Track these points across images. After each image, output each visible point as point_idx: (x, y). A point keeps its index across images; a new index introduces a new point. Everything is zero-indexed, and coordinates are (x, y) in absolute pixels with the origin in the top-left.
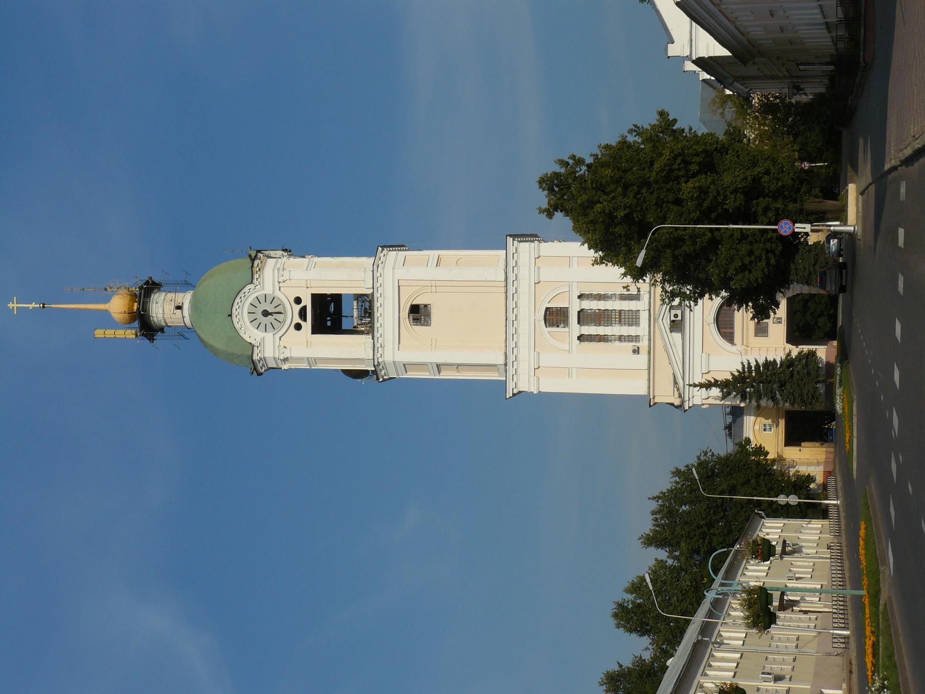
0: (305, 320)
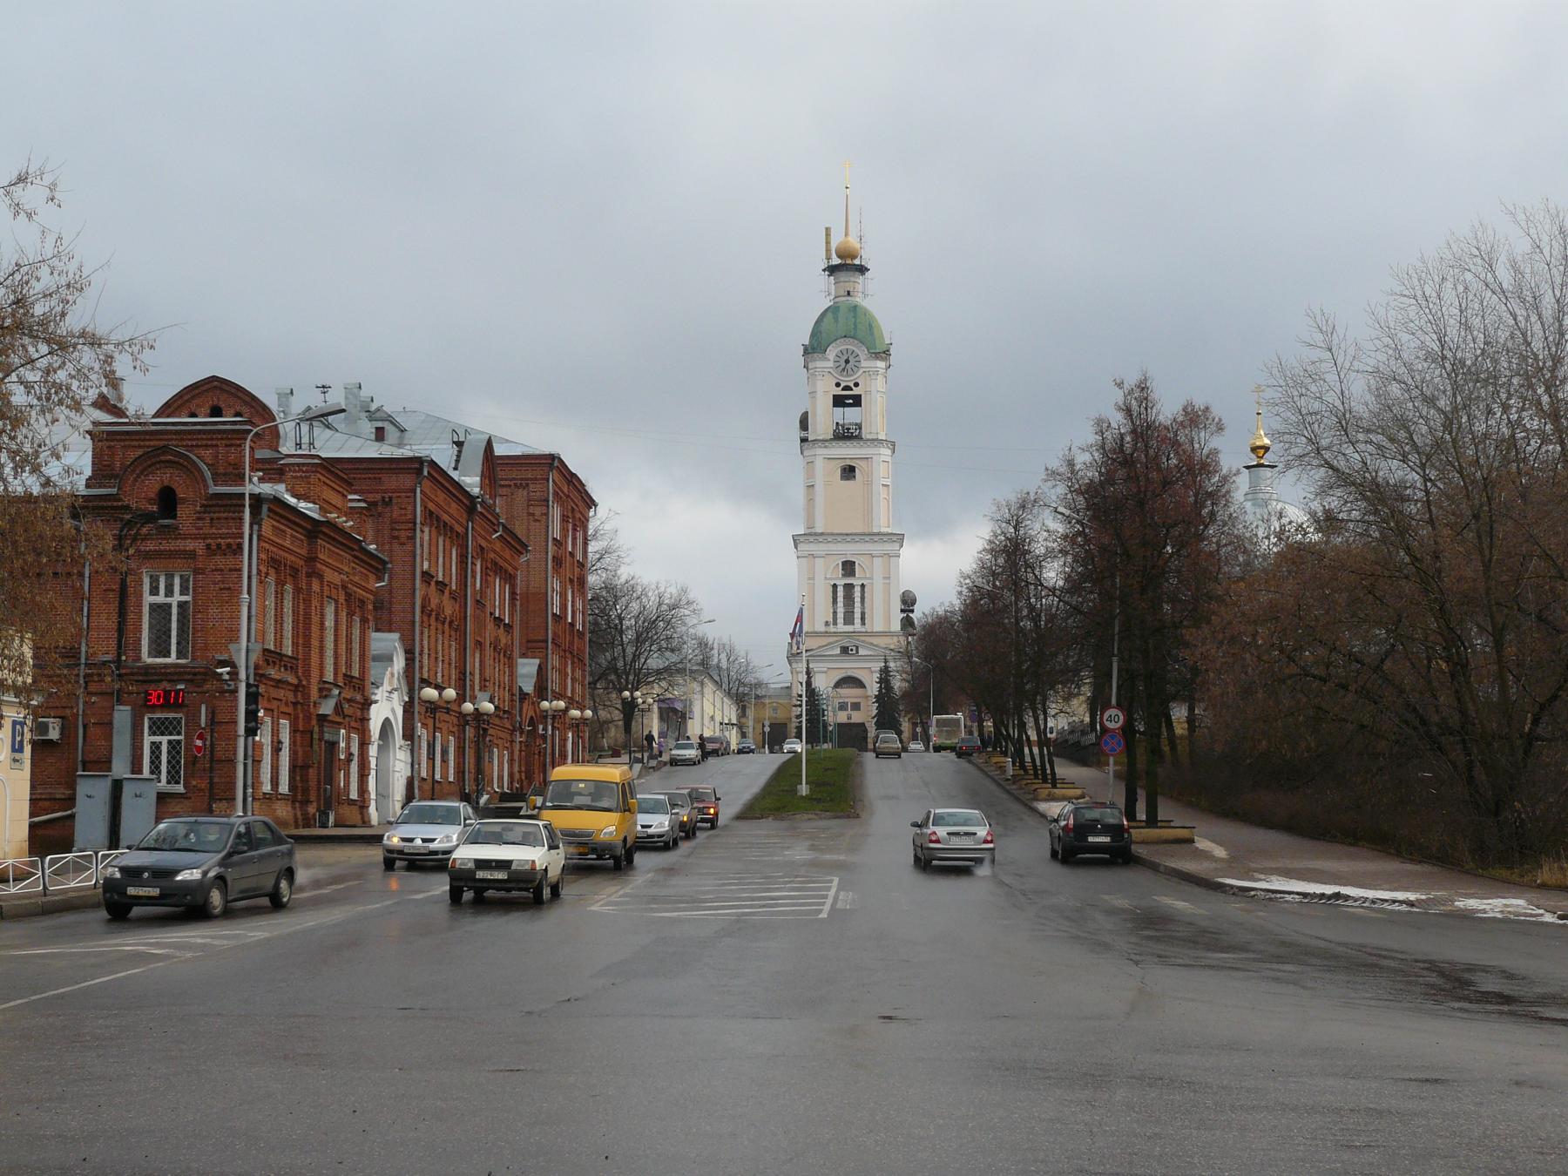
0: (843, 389)
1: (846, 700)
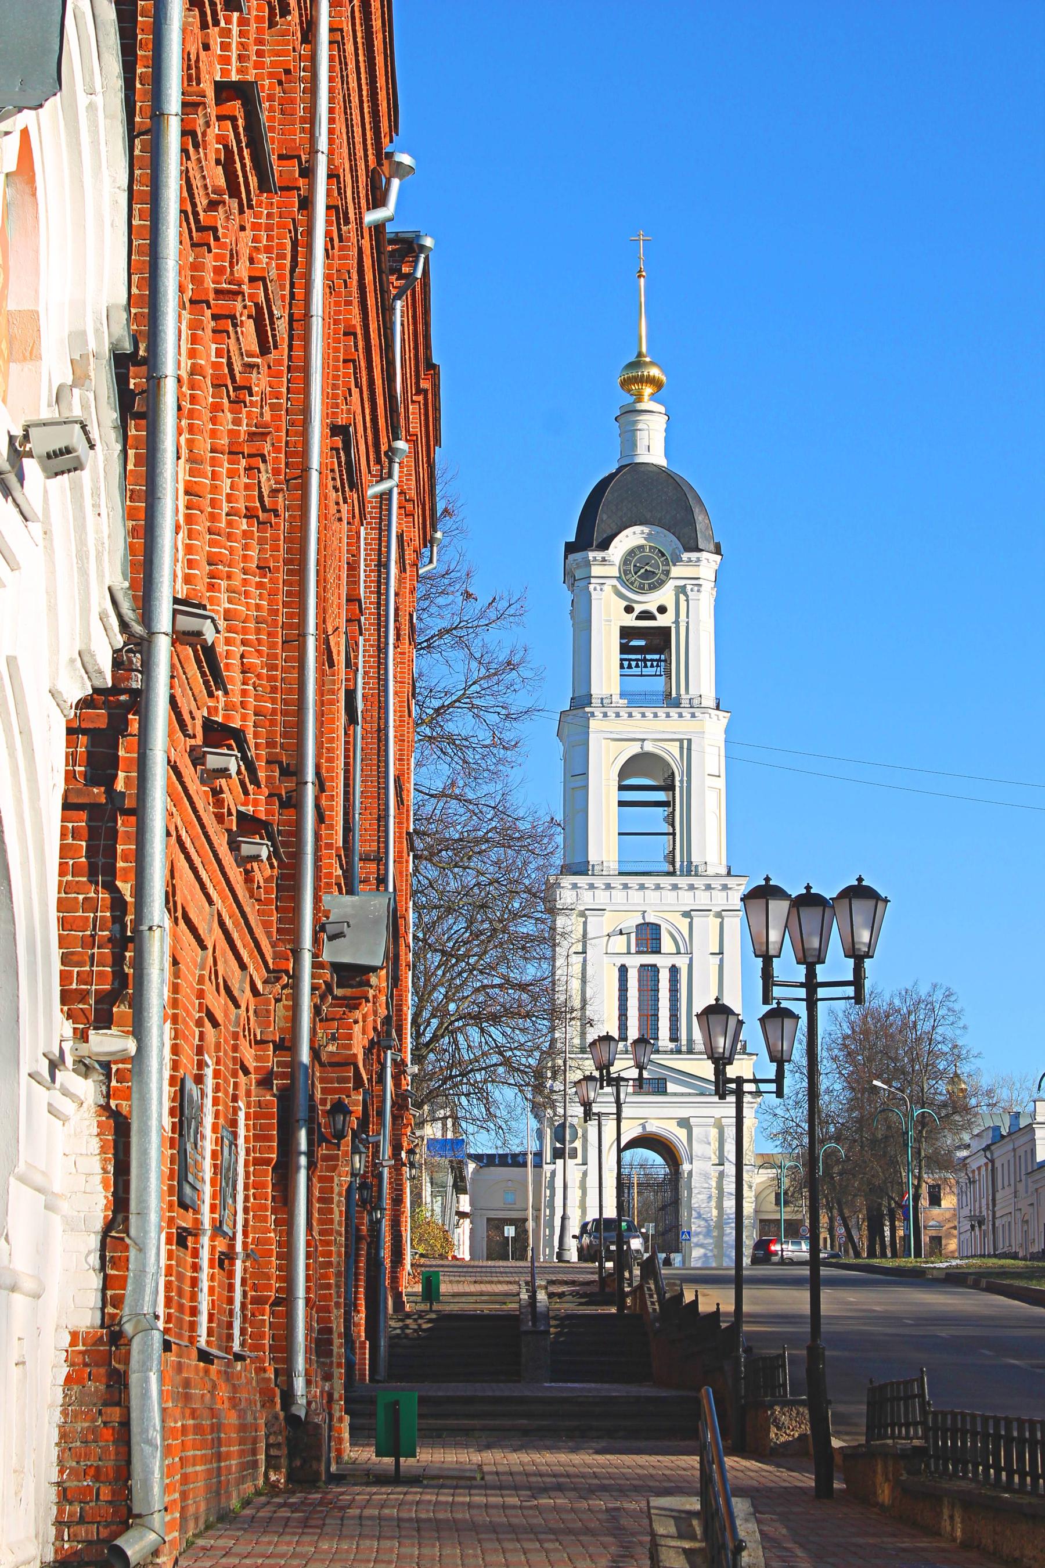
0: (638, 618)
1: (129, 1288)
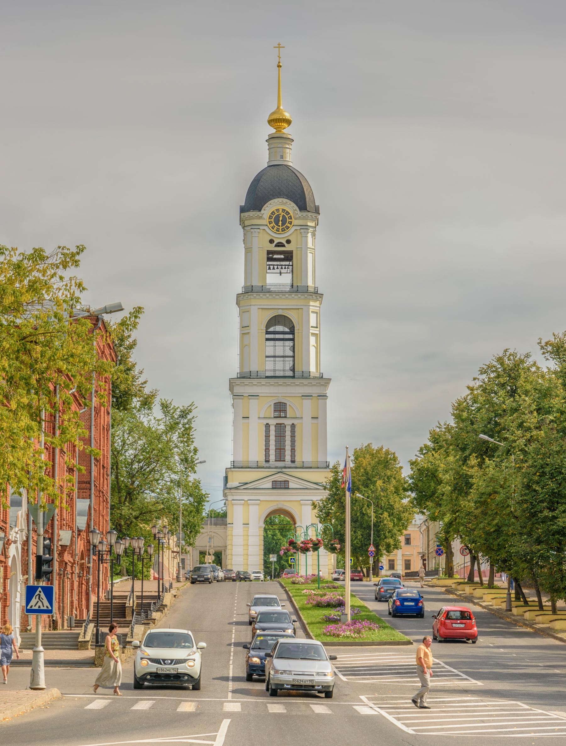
0: (276, 246)
